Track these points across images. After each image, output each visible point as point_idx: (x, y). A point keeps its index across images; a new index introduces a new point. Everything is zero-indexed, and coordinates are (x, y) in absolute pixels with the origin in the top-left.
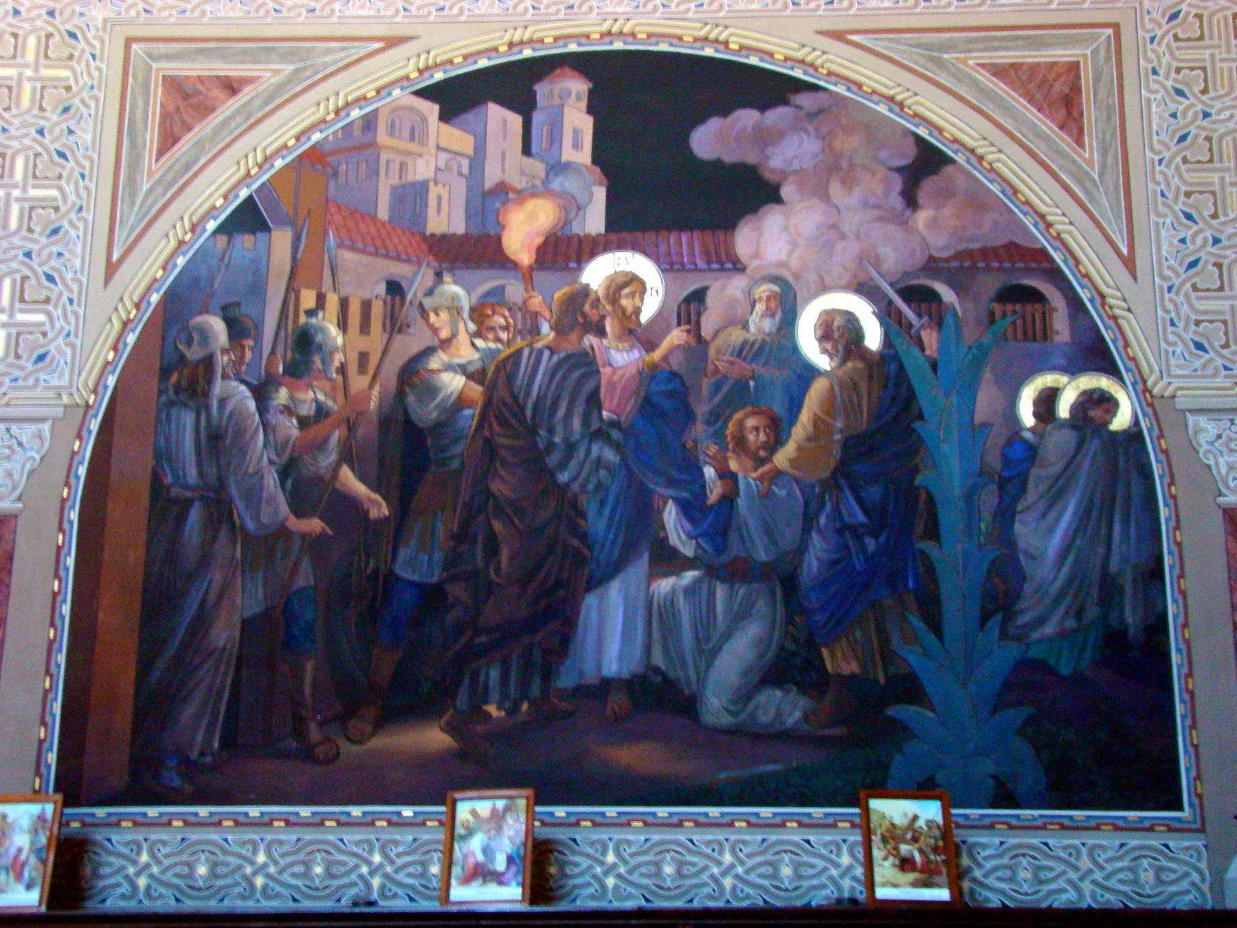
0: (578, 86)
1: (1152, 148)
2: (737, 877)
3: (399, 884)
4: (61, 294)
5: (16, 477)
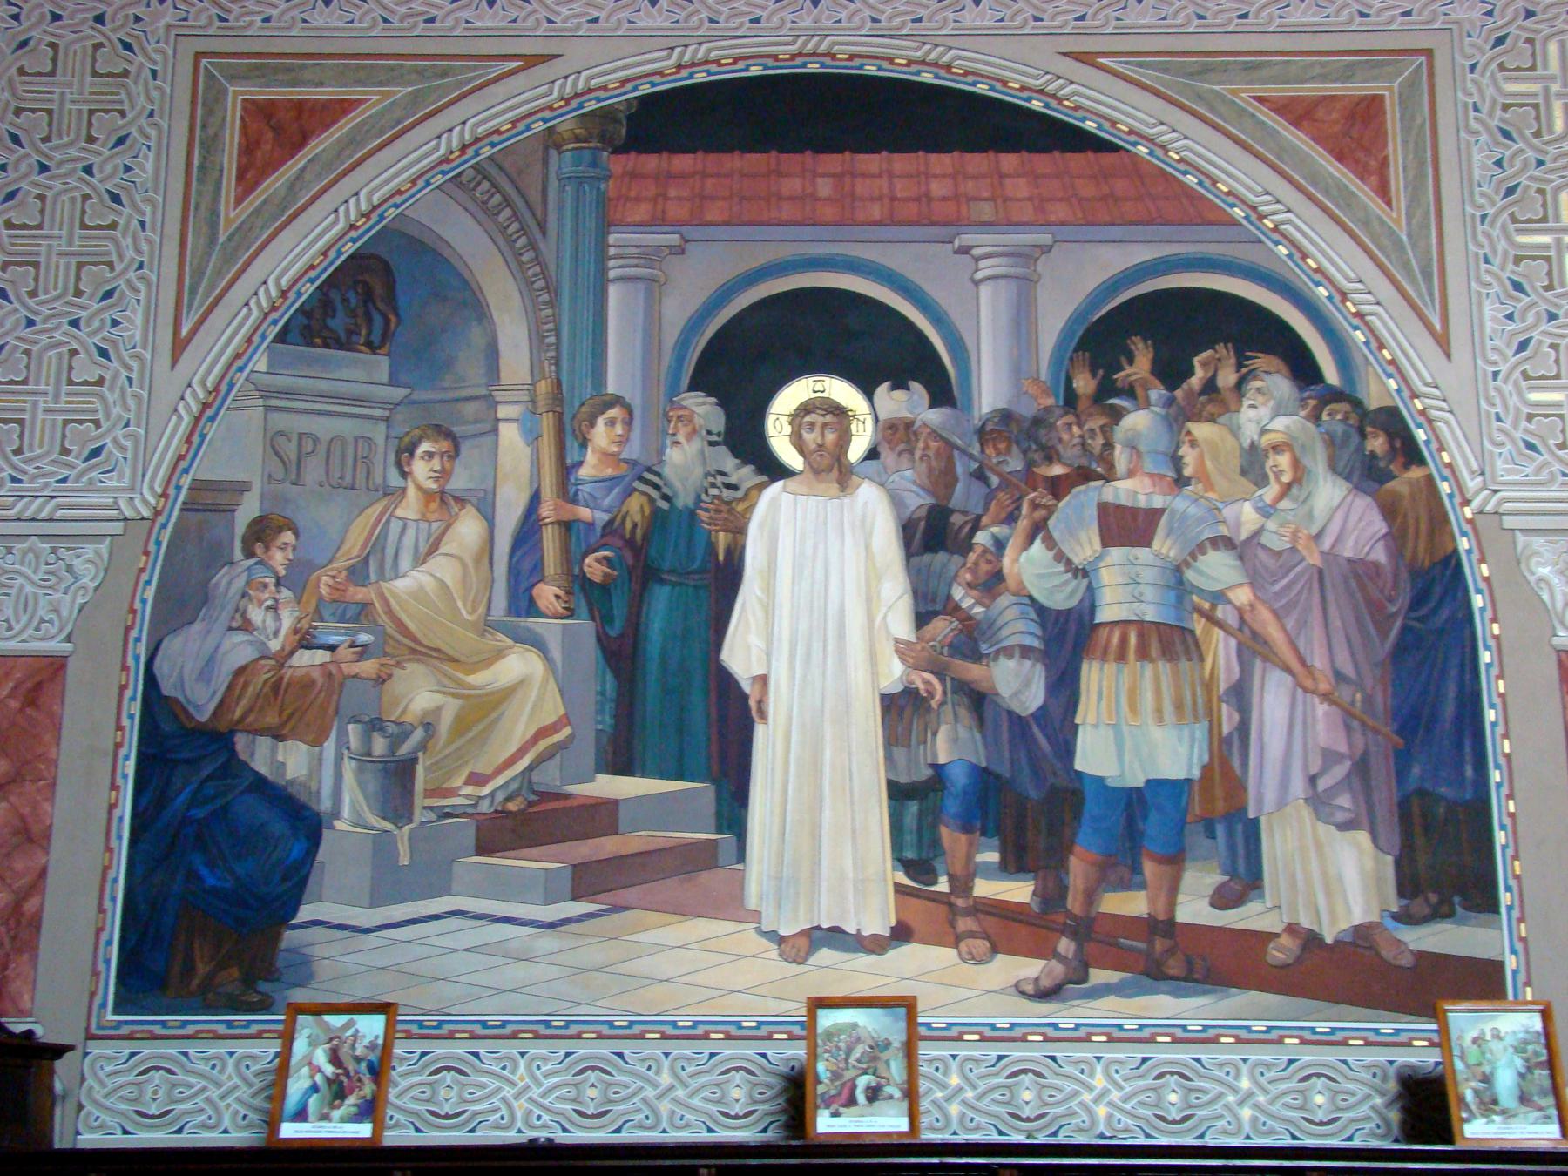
1: (1478, 279)
2: (964, 1102)
5: (65, 613)
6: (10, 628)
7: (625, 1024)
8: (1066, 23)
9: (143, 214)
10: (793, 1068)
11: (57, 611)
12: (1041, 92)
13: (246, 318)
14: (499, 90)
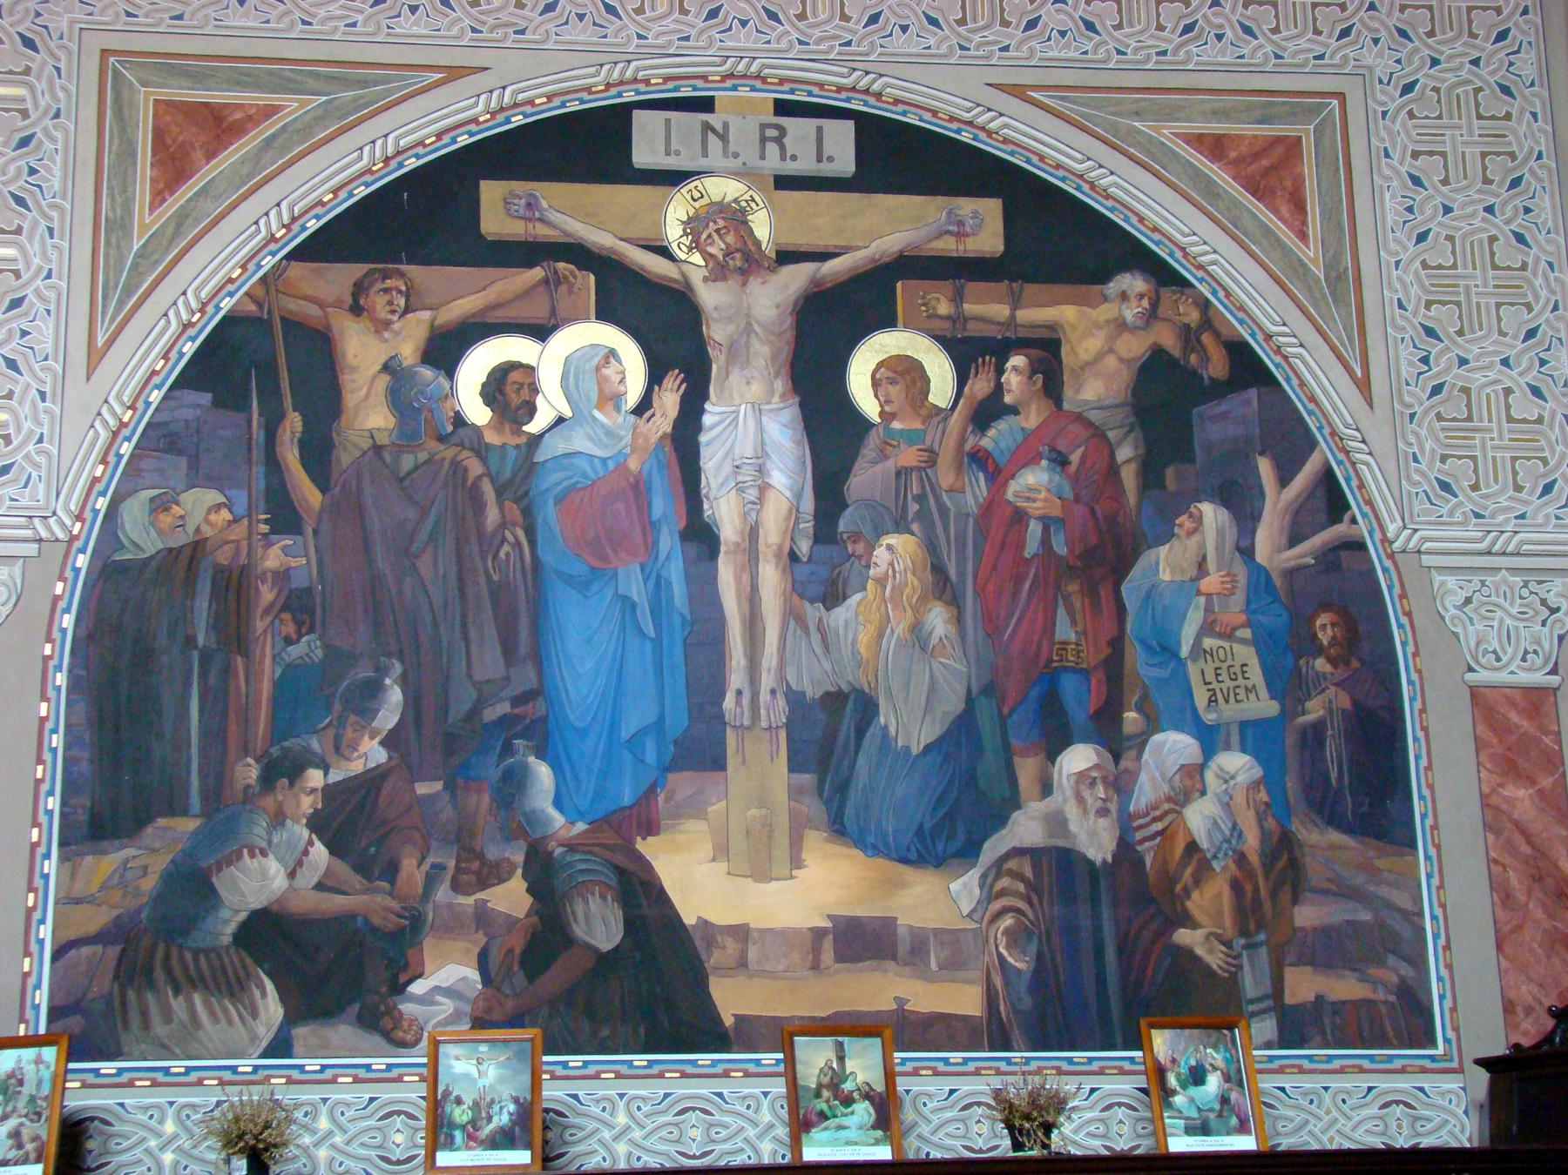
6: (1498, 659)
7: (114, 1071)
8: (670, 43)
9: (51, 219)
11: (1539, 644)
12: (970, 123)
14: (421, 102)
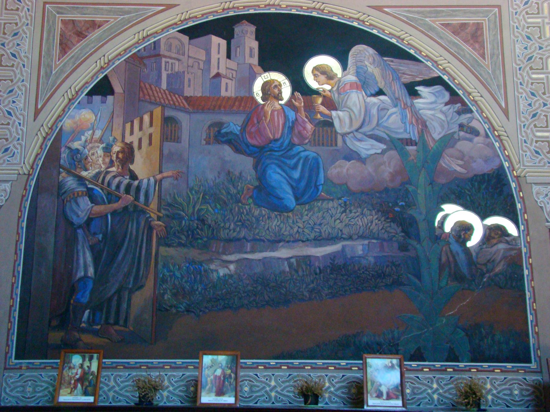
0: (252, 29)
3: (121, 395)
4: (15, 121)
10: (536, 383)
13: (63, 102)
